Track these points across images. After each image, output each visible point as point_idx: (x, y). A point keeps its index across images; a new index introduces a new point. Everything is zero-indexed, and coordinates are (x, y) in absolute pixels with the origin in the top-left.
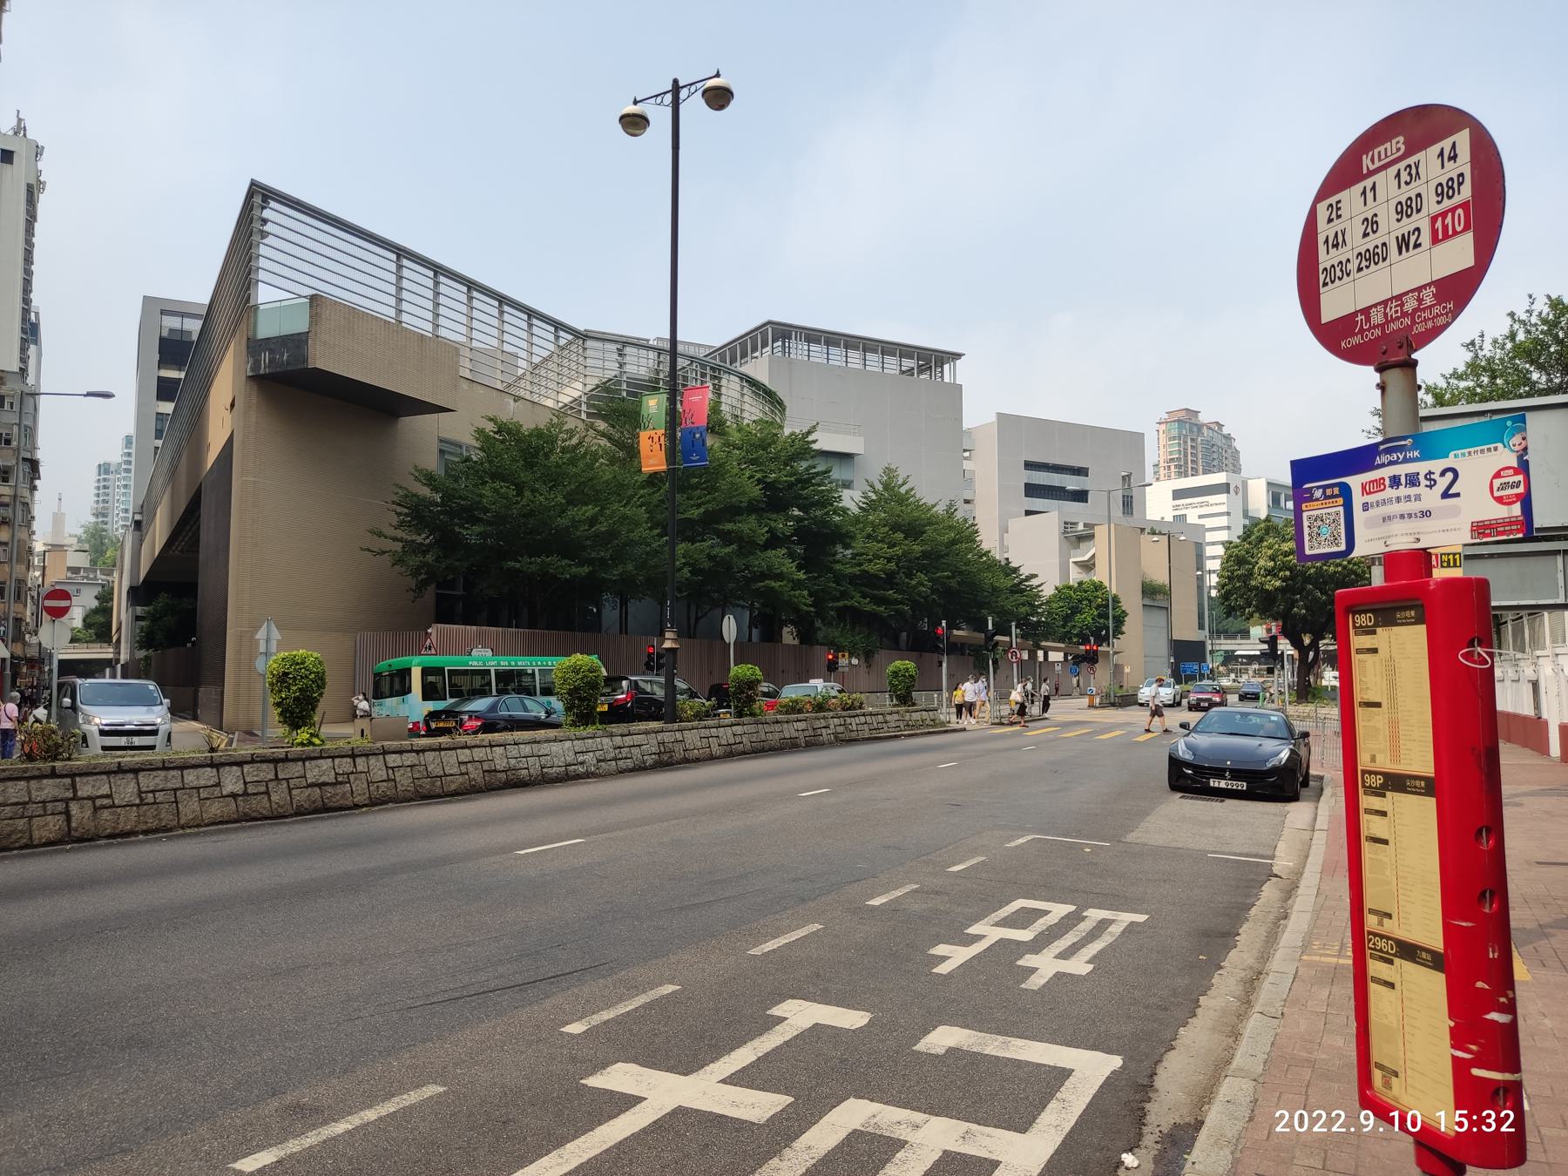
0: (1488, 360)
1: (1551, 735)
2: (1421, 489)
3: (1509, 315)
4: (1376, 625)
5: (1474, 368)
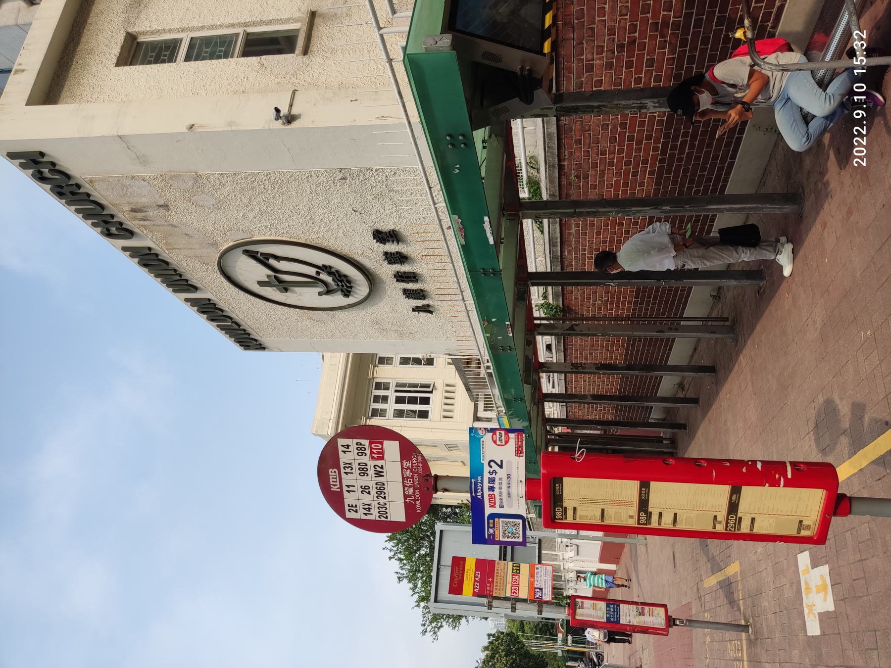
0: (409, 572)
1: (605, 568)
2: (497, 477)
3: (390, 560)
4: (562, 506)
5: (412, 579)
